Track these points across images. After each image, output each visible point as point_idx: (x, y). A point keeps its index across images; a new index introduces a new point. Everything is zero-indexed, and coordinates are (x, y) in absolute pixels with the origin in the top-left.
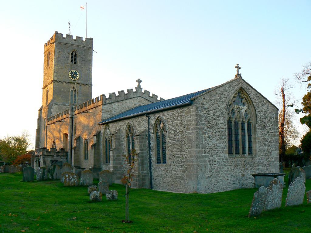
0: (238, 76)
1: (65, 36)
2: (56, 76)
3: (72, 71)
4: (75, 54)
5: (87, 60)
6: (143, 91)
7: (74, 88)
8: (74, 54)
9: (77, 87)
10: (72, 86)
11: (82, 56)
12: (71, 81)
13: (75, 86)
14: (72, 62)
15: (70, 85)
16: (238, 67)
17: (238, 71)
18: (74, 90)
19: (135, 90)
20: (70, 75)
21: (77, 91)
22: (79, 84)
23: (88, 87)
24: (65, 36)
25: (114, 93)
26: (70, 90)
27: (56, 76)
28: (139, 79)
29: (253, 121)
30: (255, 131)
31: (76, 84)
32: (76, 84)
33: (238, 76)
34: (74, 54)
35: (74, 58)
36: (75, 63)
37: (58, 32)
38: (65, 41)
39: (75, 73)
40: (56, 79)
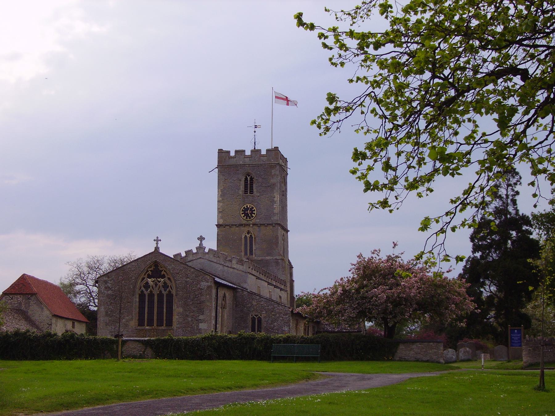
0: (157, 249)
1: (232, 154)
2: (222, 218)
3: (245, 206)
4: (252, 179)
5: (269, 185)
6: (207, 250)
7: (248, 233)
8: (249, 178)
9: (254, 231)
10: (246, 229)
11: (260, 180)
12: (244, 222)
13: (251, 229)
14: (246, 192)
15: (242, 228)
16: (157, 240)
17: (157, 244)
18: (248, 236)
19: (195, 251)
20: (242, 214)
21: (253, 236)
22: (257, 224)
23: (271, 227)
24: (232, 154)
25: (191, 251)
26: (243, 237)
27: (222, 218)
28: (201, 236)
29: (174, 292)
30: (269, 284)
31: (251, 225)
32: (251, 225)
33: (157, 249)
34: (249, 178)
35: (249, 187)
36: (252, 192)
37: (222, 150)
38: (232, 162)
39: (252, 210)
40: (221, 222)
